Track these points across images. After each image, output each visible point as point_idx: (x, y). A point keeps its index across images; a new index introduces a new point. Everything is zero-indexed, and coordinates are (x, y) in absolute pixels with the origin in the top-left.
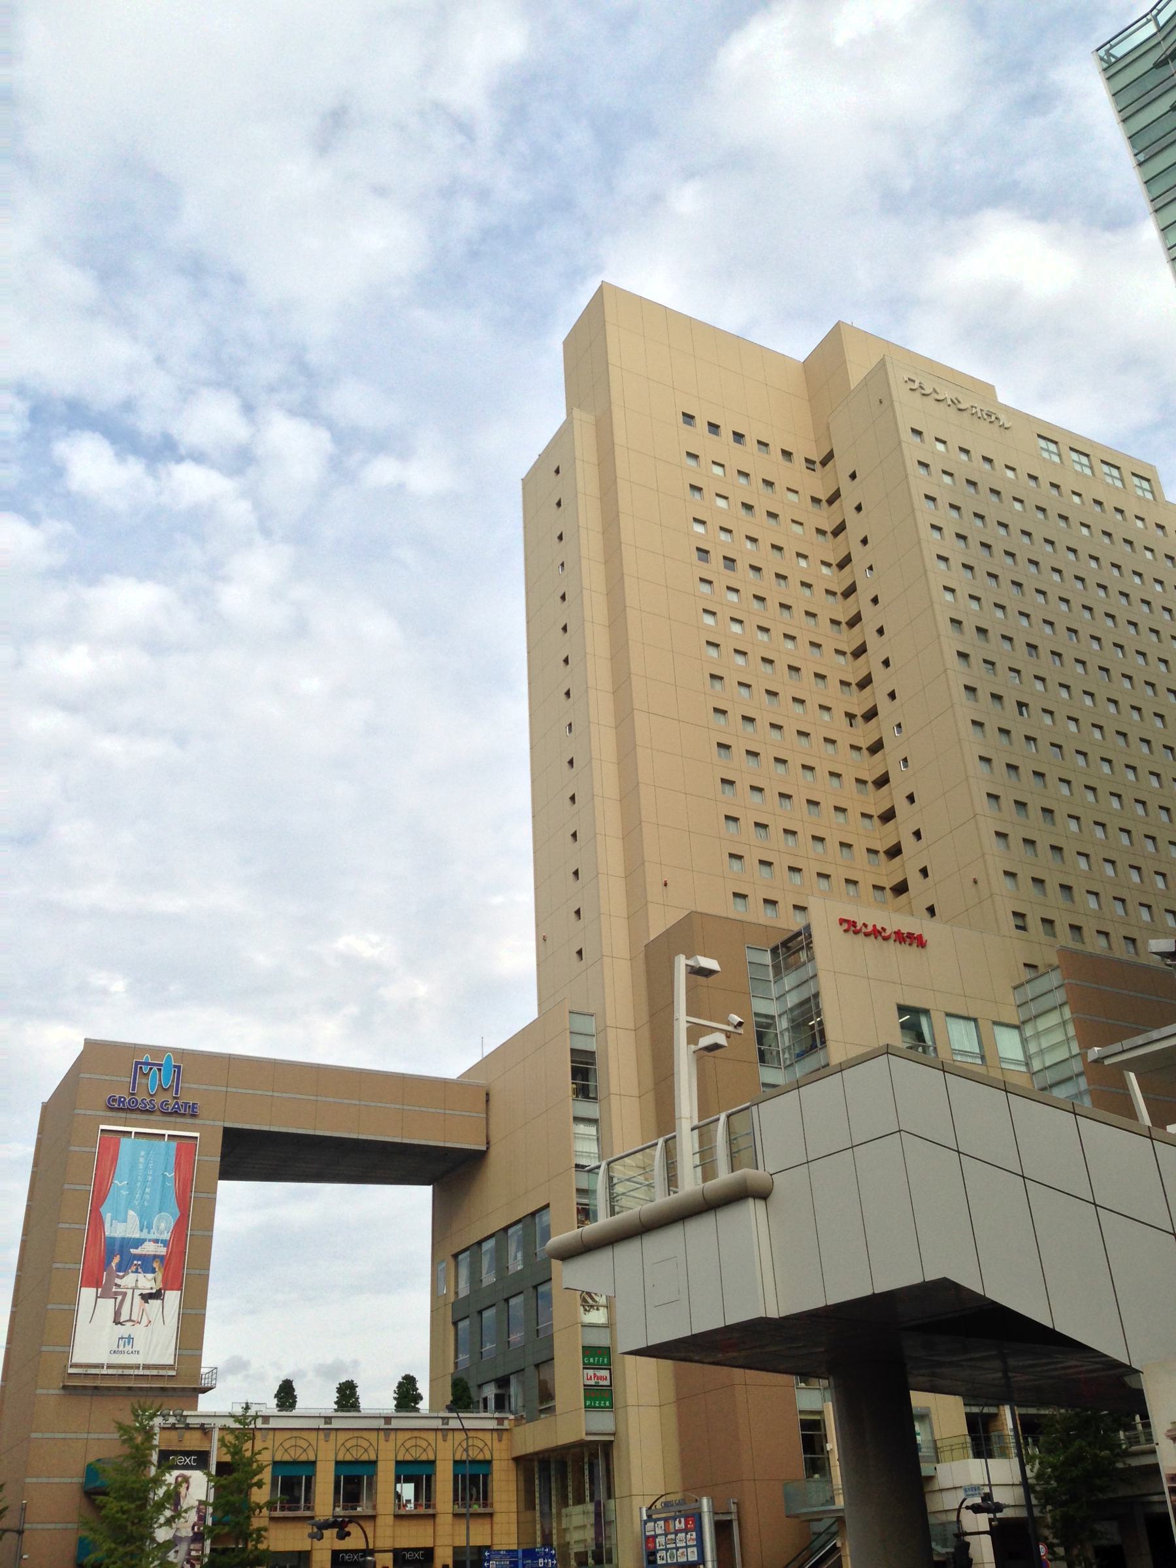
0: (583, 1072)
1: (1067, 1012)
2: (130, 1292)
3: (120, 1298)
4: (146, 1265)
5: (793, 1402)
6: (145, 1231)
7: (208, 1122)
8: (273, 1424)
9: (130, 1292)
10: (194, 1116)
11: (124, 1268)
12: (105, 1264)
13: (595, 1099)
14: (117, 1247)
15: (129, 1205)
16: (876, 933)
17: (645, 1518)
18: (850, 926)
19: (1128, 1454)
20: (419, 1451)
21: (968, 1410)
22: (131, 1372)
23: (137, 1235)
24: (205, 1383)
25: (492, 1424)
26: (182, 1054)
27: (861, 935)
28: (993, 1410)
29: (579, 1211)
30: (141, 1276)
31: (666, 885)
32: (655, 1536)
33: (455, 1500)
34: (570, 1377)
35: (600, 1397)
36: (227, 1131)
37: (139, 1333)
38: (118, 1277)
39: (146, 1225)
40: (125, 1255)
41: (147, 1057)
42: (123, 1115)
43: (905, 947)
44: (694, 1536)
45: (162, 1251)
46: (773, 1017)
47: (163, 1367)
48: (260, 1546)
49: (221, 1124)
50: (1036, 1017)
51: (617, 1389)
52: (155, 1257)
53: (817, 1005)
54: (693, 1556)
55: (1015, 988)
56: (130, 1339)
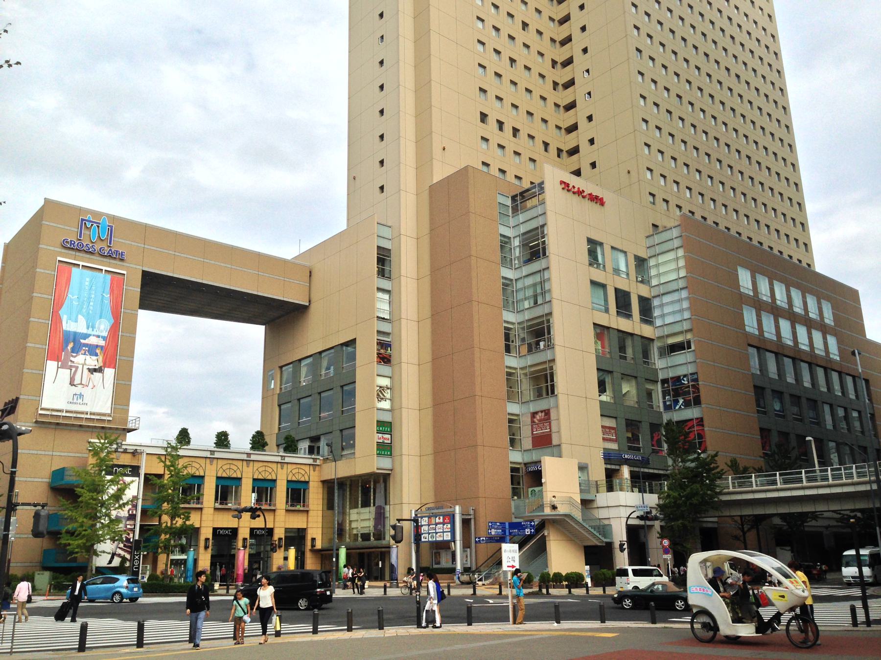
0: (384, 259)
1: (681, 252)
2: (80, 367)
3: (73, 369)
4: (92, 350)
5: (507, 456)
6: (90, 329)
9: (80, 367)
10: (122, 260)
11: (76, 350)
12: (63, 348)
14: (72, 338)
15: (79, 312)
16: (580, 193)
18: (566, 186)
19: (721, 493)
20: (267, 474)
22: (82, 416)
24: (130, 426)
26: (113, 218)
28: (617, 467)
30: (88, 357)
31: (444, 149)
34: (366, 437)
35: (385, 449)
36: (143, 271)
37: (87, 392)
40: (76, 342)
41: (89, 217)
42: (74, 253)
43: (593, 204)
44: (449, 526)
45: (102, 343)
46: (509, 238)
47: (104, 415)
48: (188, 523)
51: (396, 446)
52: (97, 346)
53: (543, 232)
54: (447, 537)
55: (647, 237)
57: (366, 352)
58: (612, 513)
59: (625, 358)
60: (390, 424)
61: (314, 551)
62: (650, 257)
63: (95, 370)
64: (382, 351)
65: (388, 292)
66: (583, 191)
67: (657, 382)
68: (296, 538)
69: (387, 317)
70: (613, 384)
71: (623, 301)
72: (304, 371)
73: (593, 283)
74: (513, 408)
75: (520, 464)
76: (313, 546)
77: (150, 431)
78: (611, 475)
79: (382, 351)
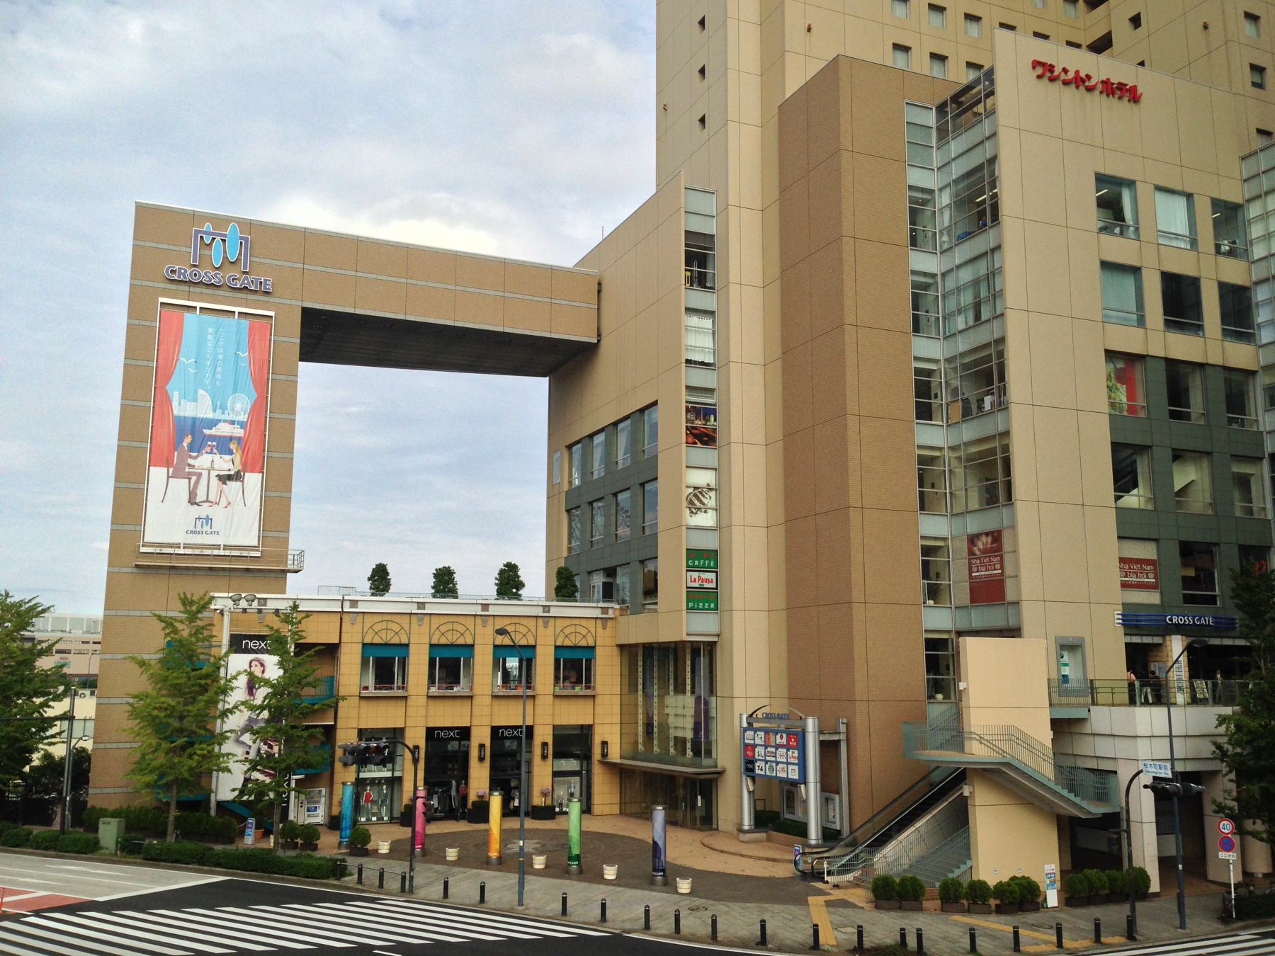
2: (205, 473)
3: (194, 478)
4: (223, 445)
6: (219, 411)
7: (283, 301)
8: (361, 608)
9: (205, 473)
11: (197, 448)
12: (176, 444)
17: (745, 725)
18: (1046, 71)
21: (1128, 639)
23: (210, 415)
25: (598, 613)
27: (1058, 84)
28: (1157, 640)
29: (688, 410)
30: (218, 456)
31: (809, 30)
32: (754, 746)
33: (557, 678)
34: (675, 578)
36: (305, 311)
37: (217, 513)
38: (191, 457)
39: (220, 405)
40: (197, 435)
42: (186, 288)
43: (1113, 101)
44: (796, 754)
45: (239, 432)
46: (931, 192)
49: (299, 303)
50: (1266, 194)
52: (231, 438)
53: (992, 173)
54: (794, 774)
56: (208, 520)
57: (672, 423)
59: (1187, 417)
60: (713, 554)
61: (606, 764)
62: (1249, 201)
63: (229, 478)
64: (699, 423)
65: (710, 313)
66: (1089, 77)
67: (1261, 459)
68: (574, 743)
69: (709, 359)
70: (1152, 473)
71: (1180, 300)
72: (598, 454)
73: (1107, 266)
74: (934, 526)
75: (948, 632)
76: (604, 755)
78: (1140, 659)
79: (699, 423)
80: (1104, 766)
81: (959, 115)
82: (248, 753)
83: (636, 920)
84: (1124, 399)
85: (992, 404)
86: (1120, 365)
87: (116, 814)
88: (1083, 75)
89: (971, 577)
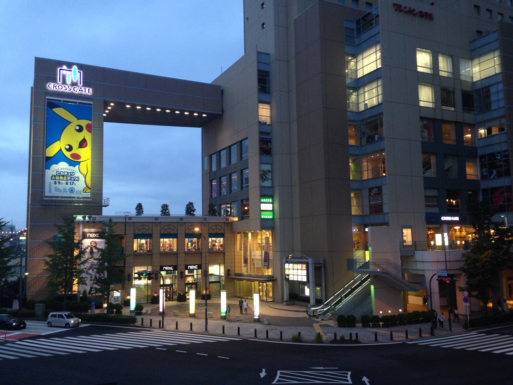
13: (269, 93)
58: (427, 266)
64: (264, 146)
66: (414, 10)
67: (476, 157)
77: (118, 203)
79: (264, 146)
80: (420, 273)
81: (364, 24)
82: (91, 277)
83: (251, 334)
84: (427, 136)
85: (378, 139)
86: (425, 122)
87: (40, 302)
88: (412, 9)
89: (370, 204)
